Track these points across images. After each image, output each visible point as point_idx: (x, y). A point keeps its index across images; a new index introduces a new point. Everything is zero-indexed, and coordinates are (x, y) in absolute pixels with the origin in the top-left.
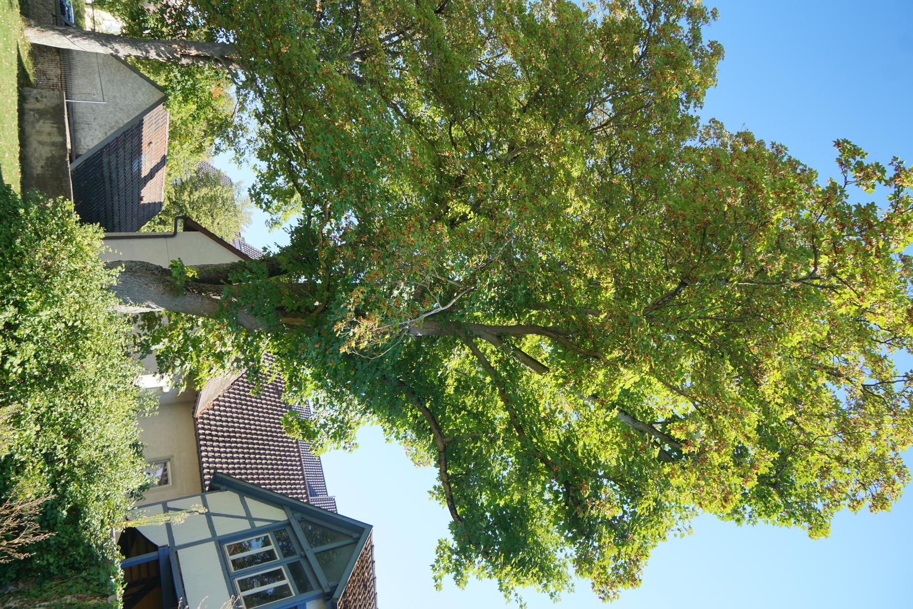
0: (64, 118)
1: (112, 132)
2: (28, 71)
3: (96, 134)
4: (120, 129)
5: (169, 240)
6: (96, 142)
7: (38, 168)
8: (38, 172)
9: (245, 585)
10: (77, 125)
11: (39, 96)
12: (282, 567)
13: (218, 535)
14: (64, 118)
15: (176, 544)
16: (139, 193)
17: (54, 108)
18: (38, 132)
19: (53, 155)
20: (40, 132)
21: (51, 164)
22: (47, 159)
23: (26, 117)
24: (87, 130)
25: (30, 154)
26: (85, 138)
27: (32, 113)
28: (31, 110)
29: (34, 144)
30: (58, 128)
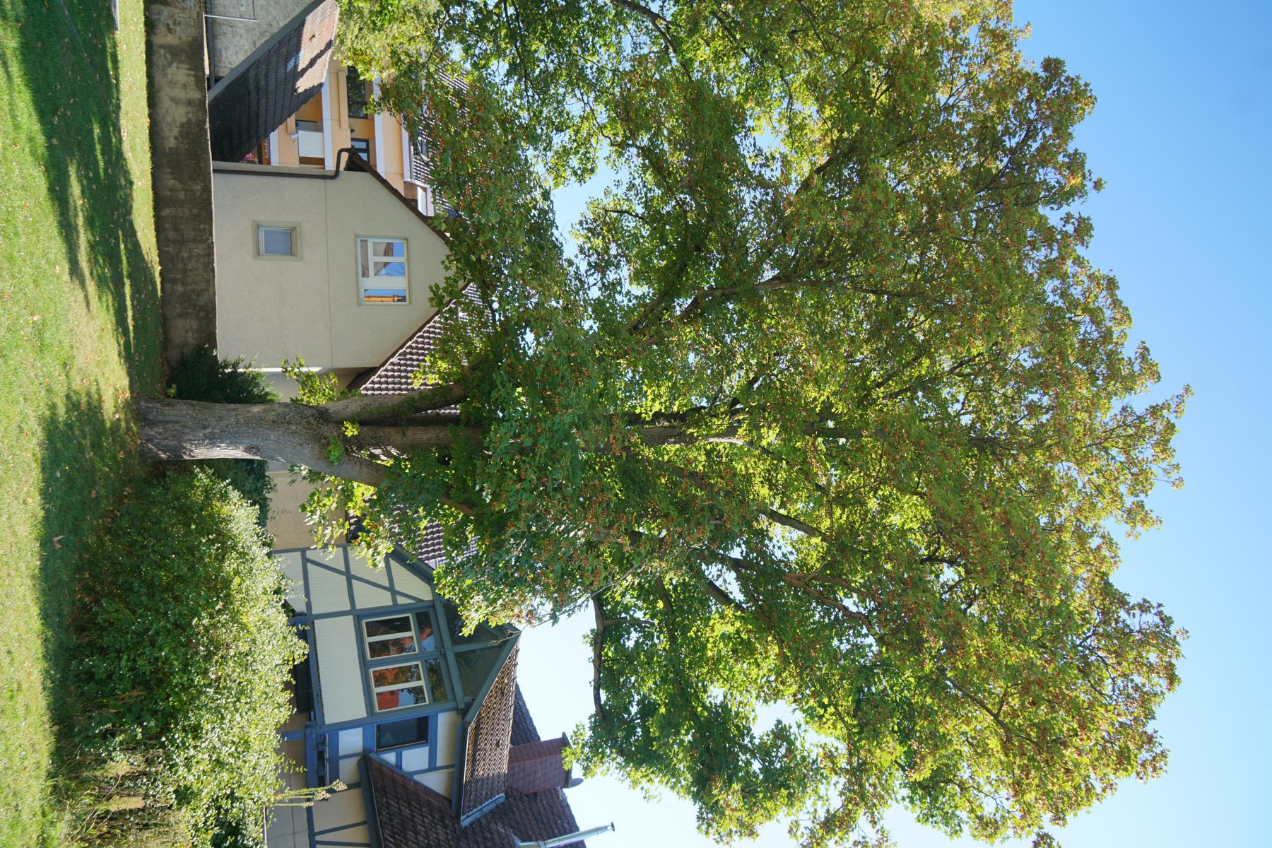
0: (203, 60)
1: (263, 40)
2: (166, 129)
4: (273, 36)
5: (329, 182)
6: (242, 57)
8: (171, 145)
9: (381, 679)
10: (217, 28)
11: (170, 22)
13: (358, 607)
15: (314, 612)
16: (294, 84)
17: (190, 45)
18: (171, 82)
21: (187, 134)
22: (182, 125)
23: (155, 58)
25: (161, 117)
27: (162, 51)
28: (162, 46)
29: (165, 103)
30: (196, 76)
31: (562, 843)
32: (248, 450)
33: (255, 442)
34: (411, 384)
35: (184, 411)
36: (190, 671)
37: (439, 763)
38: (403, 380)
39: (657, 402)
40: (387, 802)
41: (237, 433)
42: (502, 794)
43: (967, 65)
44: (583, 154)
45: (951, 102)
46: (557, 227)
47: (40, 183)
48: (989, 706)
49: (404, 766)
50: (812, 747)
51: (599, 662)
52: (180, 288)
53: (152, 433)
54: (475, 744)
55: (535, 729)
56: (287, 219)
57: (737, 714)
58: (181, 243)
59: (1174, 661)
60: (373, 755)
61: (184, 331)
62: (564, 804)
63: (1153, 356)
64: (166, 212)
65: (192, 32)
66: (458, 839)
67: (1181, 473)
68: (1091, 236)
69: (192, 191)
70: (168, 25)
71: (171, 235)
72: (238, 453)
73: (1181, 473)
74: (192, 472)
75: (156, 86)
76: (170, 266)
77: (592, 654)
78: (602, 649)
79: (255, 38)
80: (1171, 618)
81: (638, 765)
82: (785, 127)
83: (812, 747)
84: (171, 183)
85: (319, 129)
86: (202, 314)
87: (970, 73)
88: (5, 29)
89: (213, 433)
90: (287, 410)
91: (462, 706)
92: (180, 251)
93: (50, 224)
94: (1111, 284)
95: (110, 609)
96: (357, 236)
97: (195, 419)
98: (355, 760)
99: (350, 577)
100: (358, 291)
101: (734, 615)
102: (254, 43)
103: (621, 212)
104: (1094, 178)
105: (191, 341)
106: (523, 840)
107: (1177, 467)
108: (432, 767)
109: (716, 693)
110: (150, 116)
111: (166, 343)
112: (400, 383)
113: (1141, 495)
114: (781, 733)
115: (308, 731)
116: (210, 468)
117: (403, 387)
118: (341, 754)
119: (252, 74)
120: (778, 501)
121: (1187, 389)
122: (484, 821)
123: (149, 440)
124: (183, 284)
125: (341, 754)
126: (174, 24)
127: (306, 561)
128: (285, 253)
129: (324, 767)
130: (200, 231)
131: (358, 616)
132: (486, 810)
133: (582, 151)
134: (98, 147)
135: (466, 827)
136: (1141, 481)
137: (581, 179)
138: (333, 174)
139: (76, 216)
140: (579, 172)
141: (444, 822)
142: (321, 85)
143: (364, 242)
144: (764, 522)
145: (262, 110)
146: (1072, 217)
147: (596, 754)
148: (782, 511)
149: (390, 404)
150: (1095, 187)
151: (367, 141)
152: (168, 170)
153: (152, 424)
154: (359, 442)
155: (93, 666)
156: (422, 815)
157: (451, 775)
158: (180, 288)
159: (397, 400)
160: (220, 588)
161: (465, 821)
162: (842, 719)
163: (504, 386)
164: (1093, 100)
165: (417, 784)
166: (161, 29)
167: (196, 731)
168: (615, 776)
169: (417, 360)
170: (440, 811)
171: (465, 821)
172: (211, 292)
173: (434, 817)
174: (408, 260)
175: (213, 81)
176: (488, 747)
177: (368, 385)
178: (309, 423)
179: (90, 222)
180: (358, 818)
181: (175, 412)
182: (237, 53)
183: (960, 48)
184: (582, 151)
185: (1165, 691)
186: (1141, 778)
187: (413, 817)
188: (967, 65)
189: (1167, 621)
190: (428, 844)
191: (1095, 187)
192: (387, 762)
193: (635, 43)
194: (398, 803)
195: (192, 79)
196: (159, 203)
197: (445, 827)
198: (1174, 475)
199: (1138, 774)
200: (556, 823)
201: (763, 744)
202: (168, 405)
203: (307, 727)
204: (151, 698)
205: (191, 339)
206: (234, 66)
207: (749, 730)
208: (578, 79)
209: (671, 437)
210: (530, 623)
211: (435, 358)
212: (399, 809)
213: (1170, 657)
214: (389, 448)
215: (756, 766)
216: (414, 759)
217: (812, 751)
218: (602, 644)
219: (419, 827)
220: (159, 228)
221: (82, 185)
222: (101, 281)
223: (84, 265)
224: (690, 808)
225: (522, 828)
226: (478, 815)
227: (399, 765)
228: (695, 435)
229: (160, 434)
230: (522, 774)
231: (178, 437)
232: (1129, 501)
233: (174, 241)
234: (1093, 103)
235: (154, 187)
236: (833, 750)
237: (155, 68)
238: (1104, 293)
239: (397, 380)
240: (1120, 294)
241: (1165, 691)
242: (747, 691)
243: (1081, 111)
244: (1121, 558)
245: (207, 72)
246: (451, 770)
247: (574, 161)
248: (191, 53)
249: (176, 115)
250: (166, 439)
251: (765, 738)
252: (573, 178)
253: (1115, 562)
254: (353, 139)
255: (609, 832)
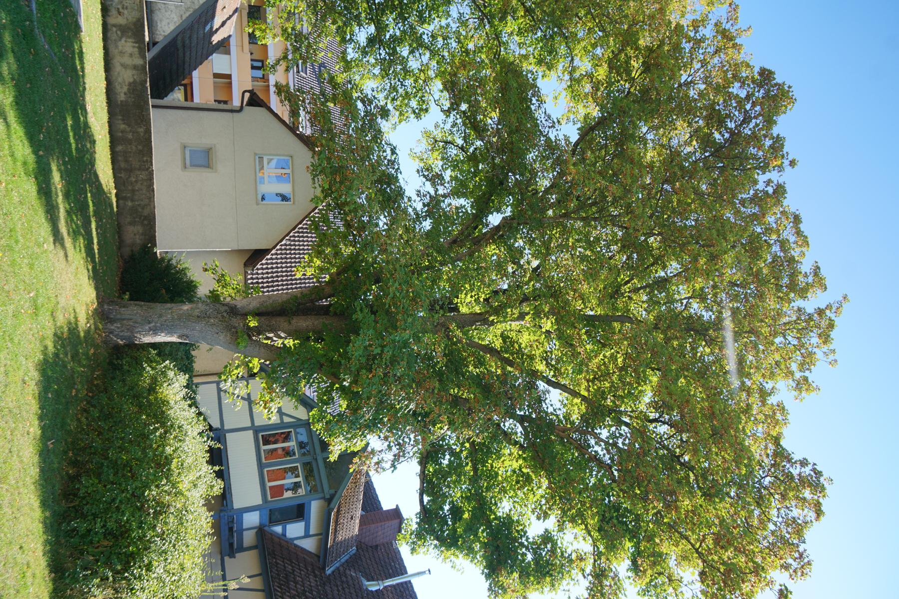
1: (188, 14)
2: (118, 87)
3: (172, 16)
4: (195, 11)
5: (235, 114)
6: (172, 27)
7: (121, 96)
9: (274, 476)
11: (120, 7)
12: (298, 464)
13: (256, 425)
14: (144, 31)
15: (226, 427)
16: (210, 38)
17: (135, 24)
19: (135, 79)
20: (122, 53)
22: (130, 84)
23: (109, 35)
24: (163, 11)
25: (114, 78)
26: (161, 21)
27: (114, 29)
28: (114, 26)
29: (117, 68)
30: (139, 48)
31: (394, 583)
32: (179, 337)
33: (185, 332)
34: (295, 275)
35: (134, 311)
36: (144, 527)
37: (312, 532)
38: (288, 252)
39: (469, 296)
40: (276, 562)
41: (173, 326)
42: (354, 548)
43: (702, 54)
44: (420, 98)
45: (689, 80)
46: (401, 173)
47: (30, 187)
48: (692, 541)
49: (287, 534)
50: (568, 545)
51: (423, 476)
52: (130, 204)
53: (113, 328)
54: (336, 522)
55: (377, 496)
56: (205, 142)
57: (518, 521)
58: (130, 171)
59: (821, 500)
60: (266, 528)
61: (133, 234)
62: (396, 551)
63: (823, 272)
64: (119, 148)
65: (136, 14)
66: (324, 584)
67: (836, 357)
68: (785, 198)
69: (137, 132)
70: (118, 9)
71: (123, 165)
72: (174, 339)
73: (836, 357)
74: (142, 365)
75: (111, 55)
76: (123, 188)
77: (419, 471)
78: (425, 467)
79: (182, 13)
80: (821, 472)
81: (449, 547)
82: (567, 77)
83: (568, 545)
84: (123, 126)
85: (228, 52)
86: (146, 222)
87: (705, 60)
88: (4, 92)
89: (155, 326)
90: (208, 308)
91: (328, 496)
92: (130, 176)
93: (41, 217)
94: (797, 219)
95: (87, 483)
96: (256, 154)
97: (142, 316)
98: (255, 530)
100: (257, 194)
101: (518, 453)
102: (181, 16)
103: (446, 142)
104: (790, 158)
105: (138, 241)
106: (368, 581)
107: (833, 351)
108: (307, 535)
109: (504, 507)
110: (107, 79)
111: (121, 243)
112: (286, 254)
113: (807, 371)
114: (547, 538)
115: (222, 514)
116: (154, 350)
117: (288, 256)
118: (244, 527)
119: (179, 38)
120: (552, 373)
121: (845, 298)
122: (341, 569)
123: (111, 333)
124: (132, 201)
125: (244, 527)
126: (123, 8)
127: (219, 390)
128: (204, 166)
129: (233, 537)
130: (144, 162)
131: (256, 430)
132: (343, 560)
133: (419, 95)
134: (71, 134)
135: (329, 575)
136: (807, 361)
137: (418, 117)
138: (238, 109)
139: (57, 196)
140: (417, 111)
141: (314, 573)
142: (230, 36)
143: (261, 158)
144: (542, 385)
145: (187, 59)
146: (772, 182)
147: (420, 539)
148: (553, 379)
149: (280, 301)
150: (790, 165)
151: (262, 61)
152: (120, 117)
153: (112, 321)
154: (259, 331)
155: (77, 527)
156: (300, 569)
157: (320, 541)
158: (130, 204)
159: (285, 298)
160: (162, 464)
161: (329, 571)
162: (590, 535)
163: (361, 310)
164: (793, 101)
165: (296, 546)
166: (113, 12)
167: (149, 567)
168: (433, 555)
169: (299, 258)
170: (312, 565)
171: (329, 571)
172: (152, 206)
173: (308, 570)
174: (293, 171)
175: (151, 45)
176: (346, 520)
177: (264, 262)
178: (223, 316)
179: (67, 196)
180: (256, 571)
181: (129, 312)
182: (169, 24)
183: (698, 42)
184: (419, 95)
185: (814, 521)
186: (793, 579)
187: (294, 571)
188: (702, 54)
189: (818, 474)
190: (304, 590)
191: (790, 165)
192: (276, 533)
193: (459, 13)
194: (283, 562)
195: (137, 50)
196: (114, 142)
197: (315, 576)
198: (831, 357)
199: (791, 576)
200: (390, 565)
201: (534, 543)
202: (124, 307)
203: (221, 511)
204: (117, 545)
205: (138, 240)
206: (166, 34)
207: (526, 532)
208: (418, 43)
209: (478, 322)
210: (377, 471)
211: (312, 257)
212: (284, 566)
213: (819, 497)
214: (279, 333)
215: (529, 557)
216: (295, 530)
217: (568, 547)
218: (426, 464)
219: (298, 578)
220: (114, 161)
221: (61, 173)
222: (75, 234)
223: (63, 229)
224: (484, 584)
225: (367, 571)
226: (337, 565)
227: (284, 534)
228: (495, 321)
229: (118, 328)
230: (368, 534)
231: (131, 329)
232: (798, 375)
233: (125, 170)
234: (793, 103)
235: (110, 132)
236: (583, 554)
237: (110, 42)
238: (791, 224)
239: (283, 252)
240: (802, 227)
241: (814, 521)
242: (525, 506)
243: (784, 108)
244: (790, 421)
245: (147, 39)
246: (320, 537)
247: (414, 103)
248: (135, 30)
249: (125, 77)
250: (123, 331)
251: (536, 538)
252: (413, 116)
253: (785, 424)
254: (252, 60)
255: (427, 576)
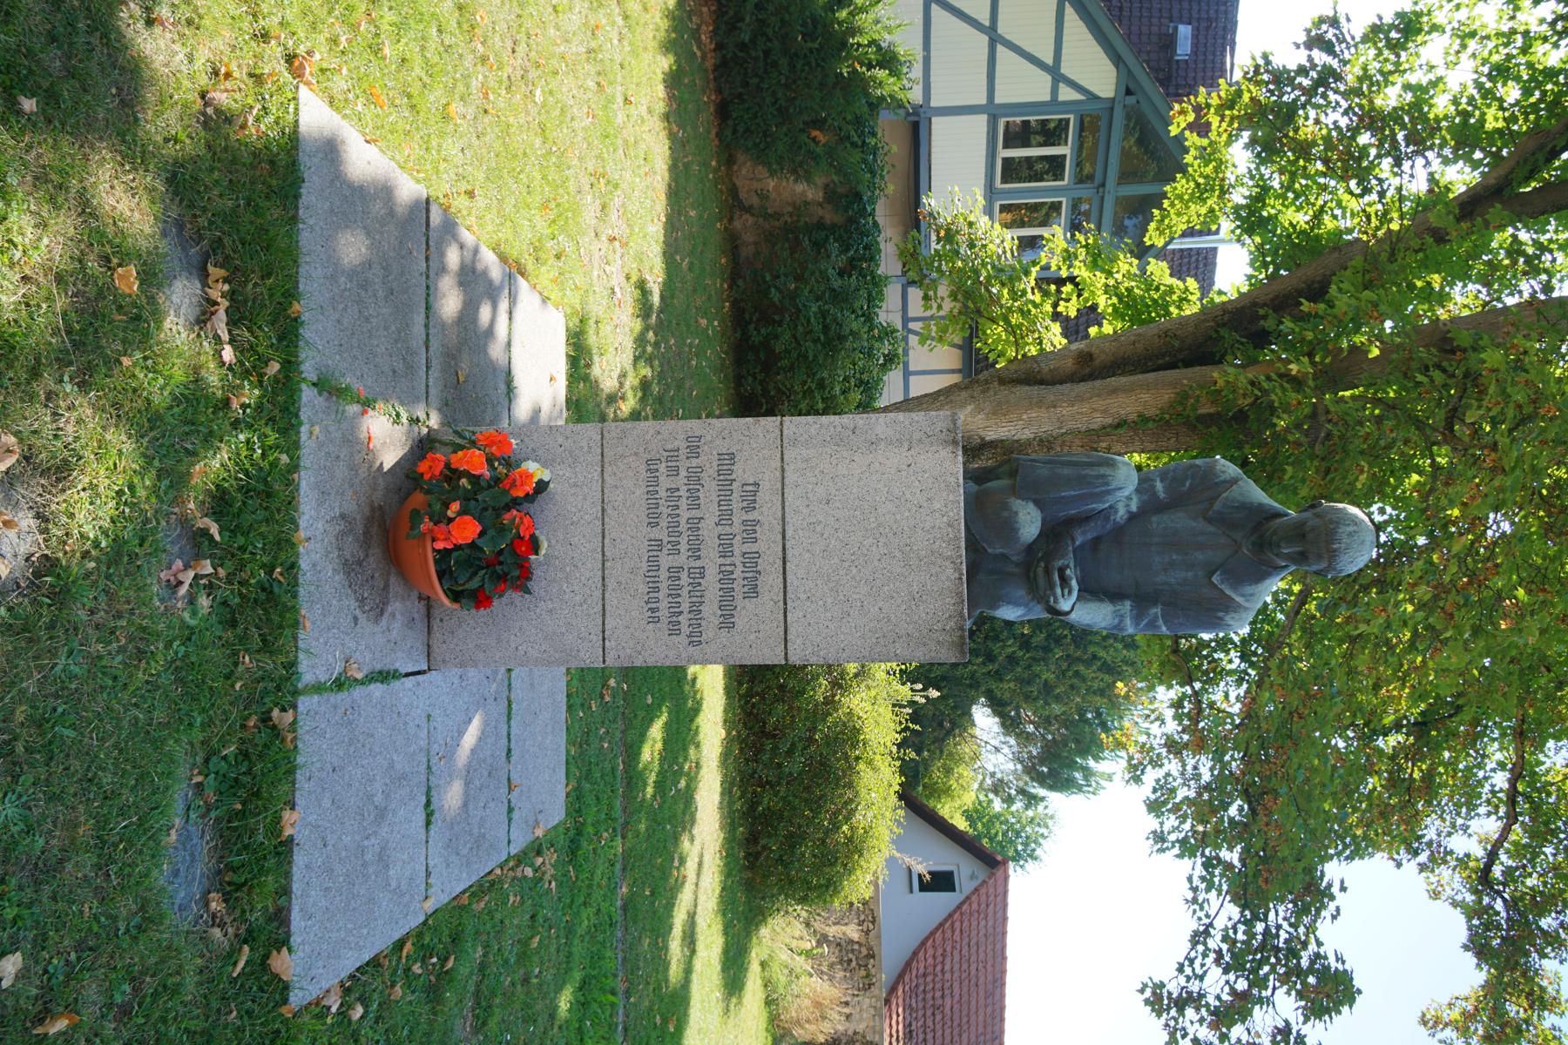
15: (933, 104)
99: (995, 40)
131: (993, 111)
